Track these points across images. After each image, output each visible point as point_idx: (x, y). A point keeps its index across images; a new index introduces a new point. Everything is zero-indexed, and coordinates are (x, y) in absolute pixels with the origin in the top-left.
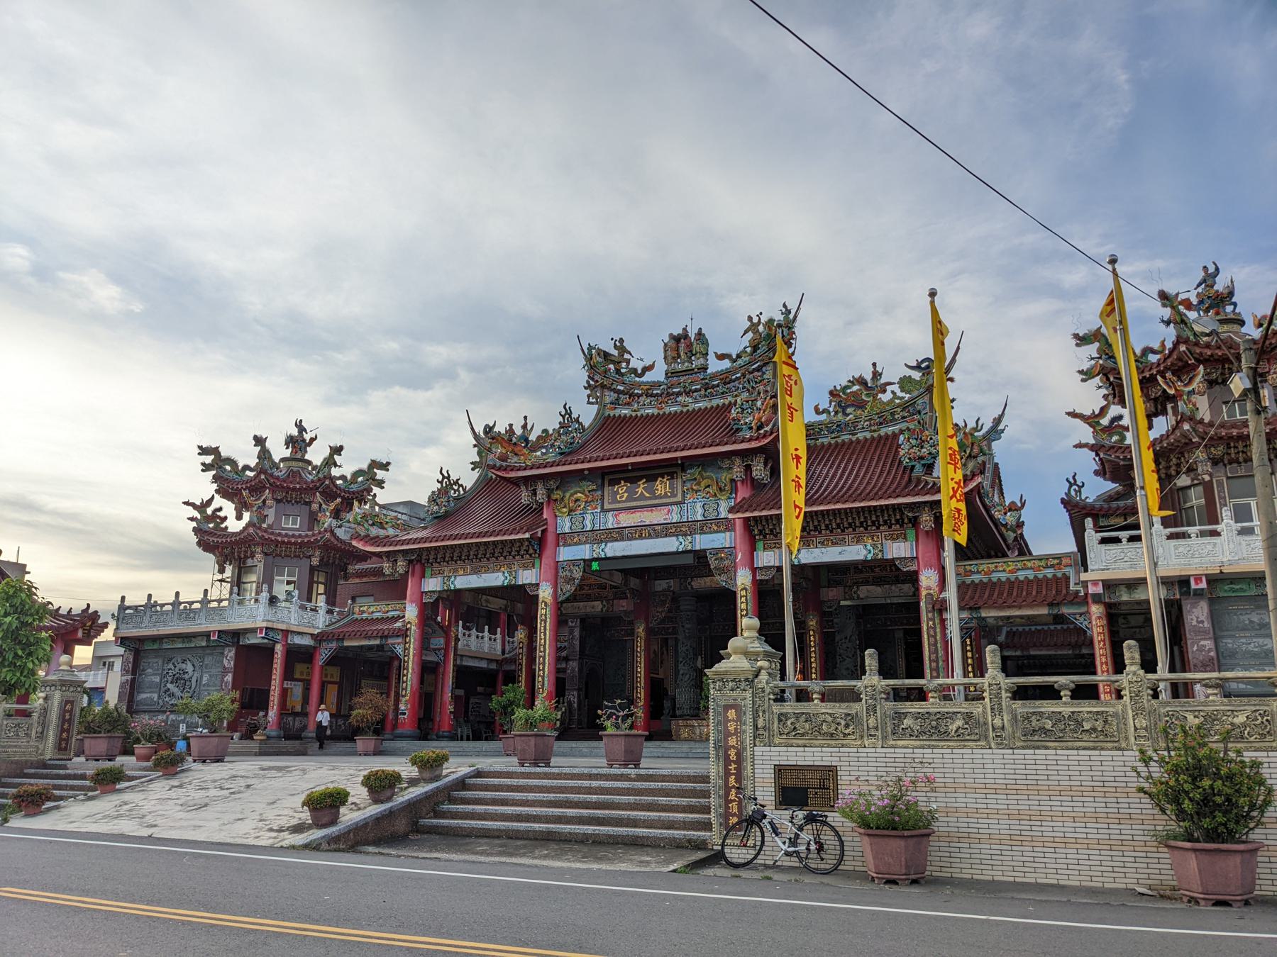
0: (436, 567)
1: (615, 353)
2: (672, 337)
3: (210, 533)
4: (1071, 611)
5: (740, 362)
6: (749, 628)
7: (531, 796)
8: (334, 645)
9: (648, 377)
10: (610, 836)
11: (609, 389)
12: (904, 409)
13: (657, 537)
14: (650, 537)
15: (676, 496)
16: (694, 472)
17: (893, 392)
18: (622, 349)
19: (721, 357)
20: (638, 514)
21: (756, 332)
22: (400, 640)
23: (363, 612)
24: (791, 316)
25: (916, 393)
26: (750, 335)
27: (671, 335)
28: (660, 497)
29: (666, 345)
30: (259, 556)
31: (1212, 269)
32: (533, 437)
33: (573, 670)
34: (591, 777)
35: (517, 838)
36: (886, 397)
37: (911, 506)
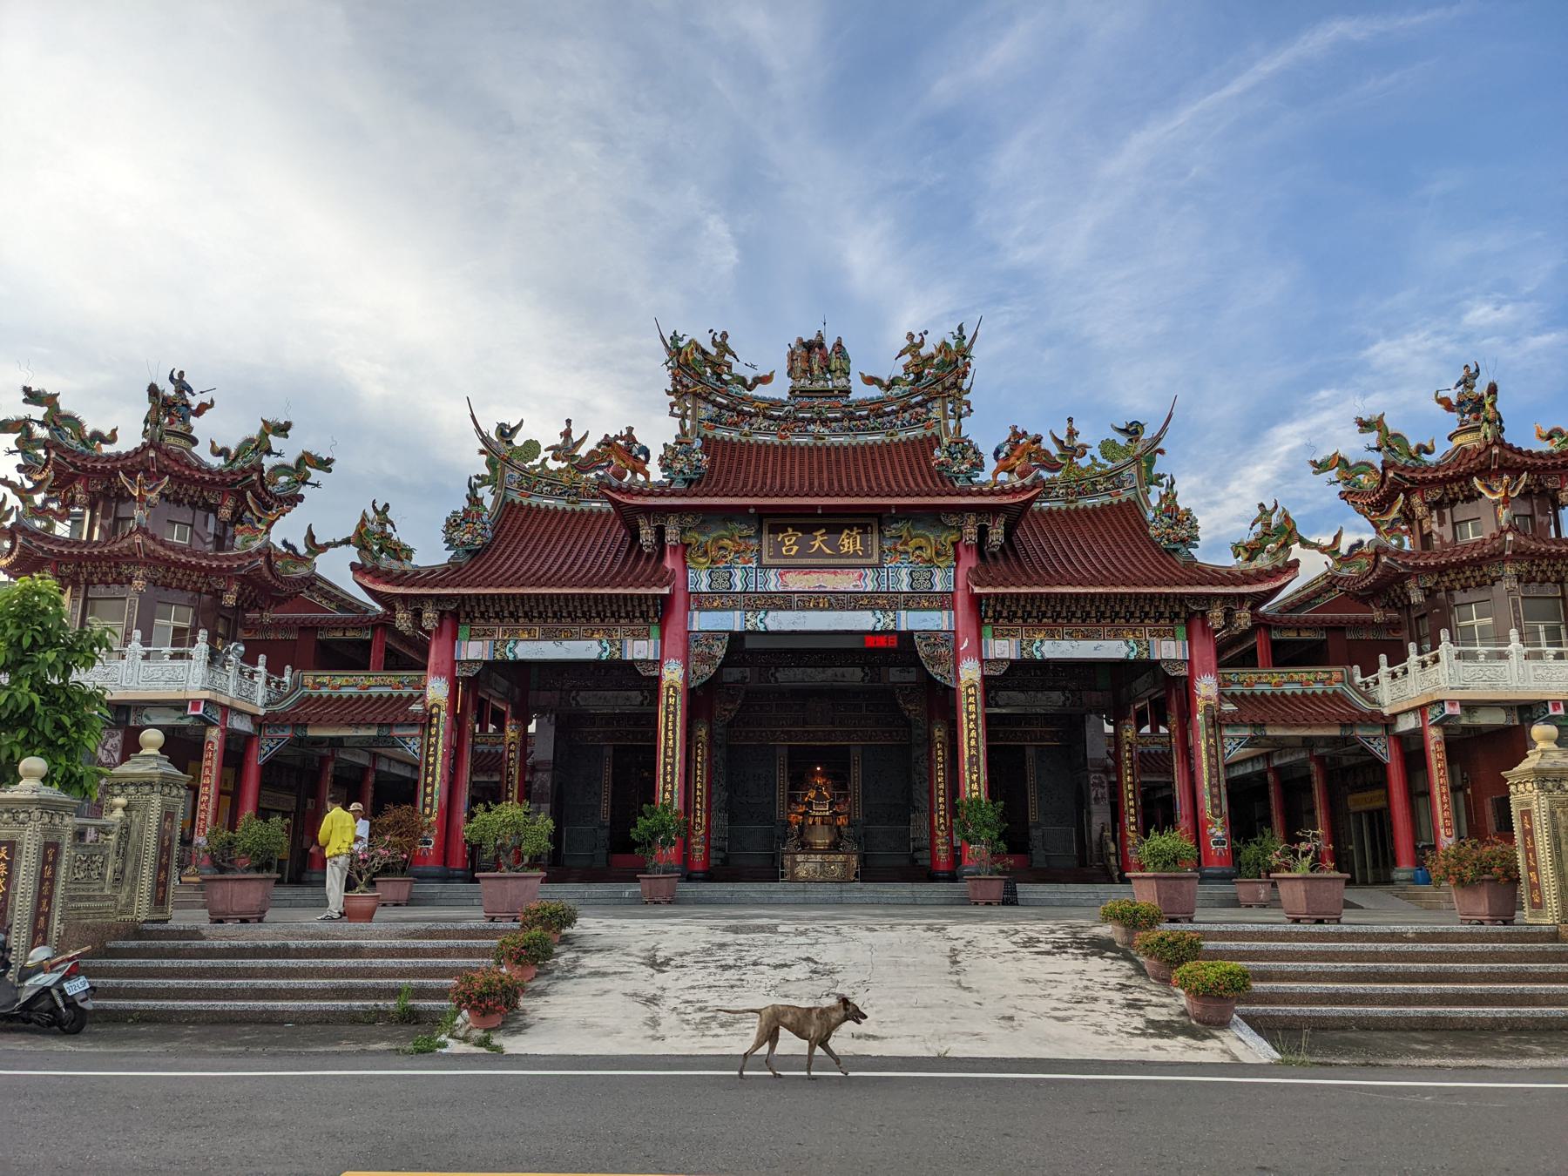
0: (480, 625)
1: (713, 351)
2: (801, 343)
3: (35, 534)
4: (1365, 734)
5: (896, 390)
6: (1547, 739)
7: (1312, 966)
8: (287, 733)
9: (760, 391)
10: (1538, 1020)
11: (706, 399)
12: (1108, 479)
13: (842, 609)
14: (831, 608)
15: (870, 556)
16: (902, 528)
18: (723, 347)
19: (870, 381)
22: (416, 731)
23: (323, 685)
24: (966, 342)
25: (1121, 462)
26: (907, 358)
27: (800, 339)
28: (847, 555)
29: (793, 352)
30: (139, 584)
31: (1472, 370)
34: (1264, 936)
35: (1378, 1029)
36: (1084, 462)
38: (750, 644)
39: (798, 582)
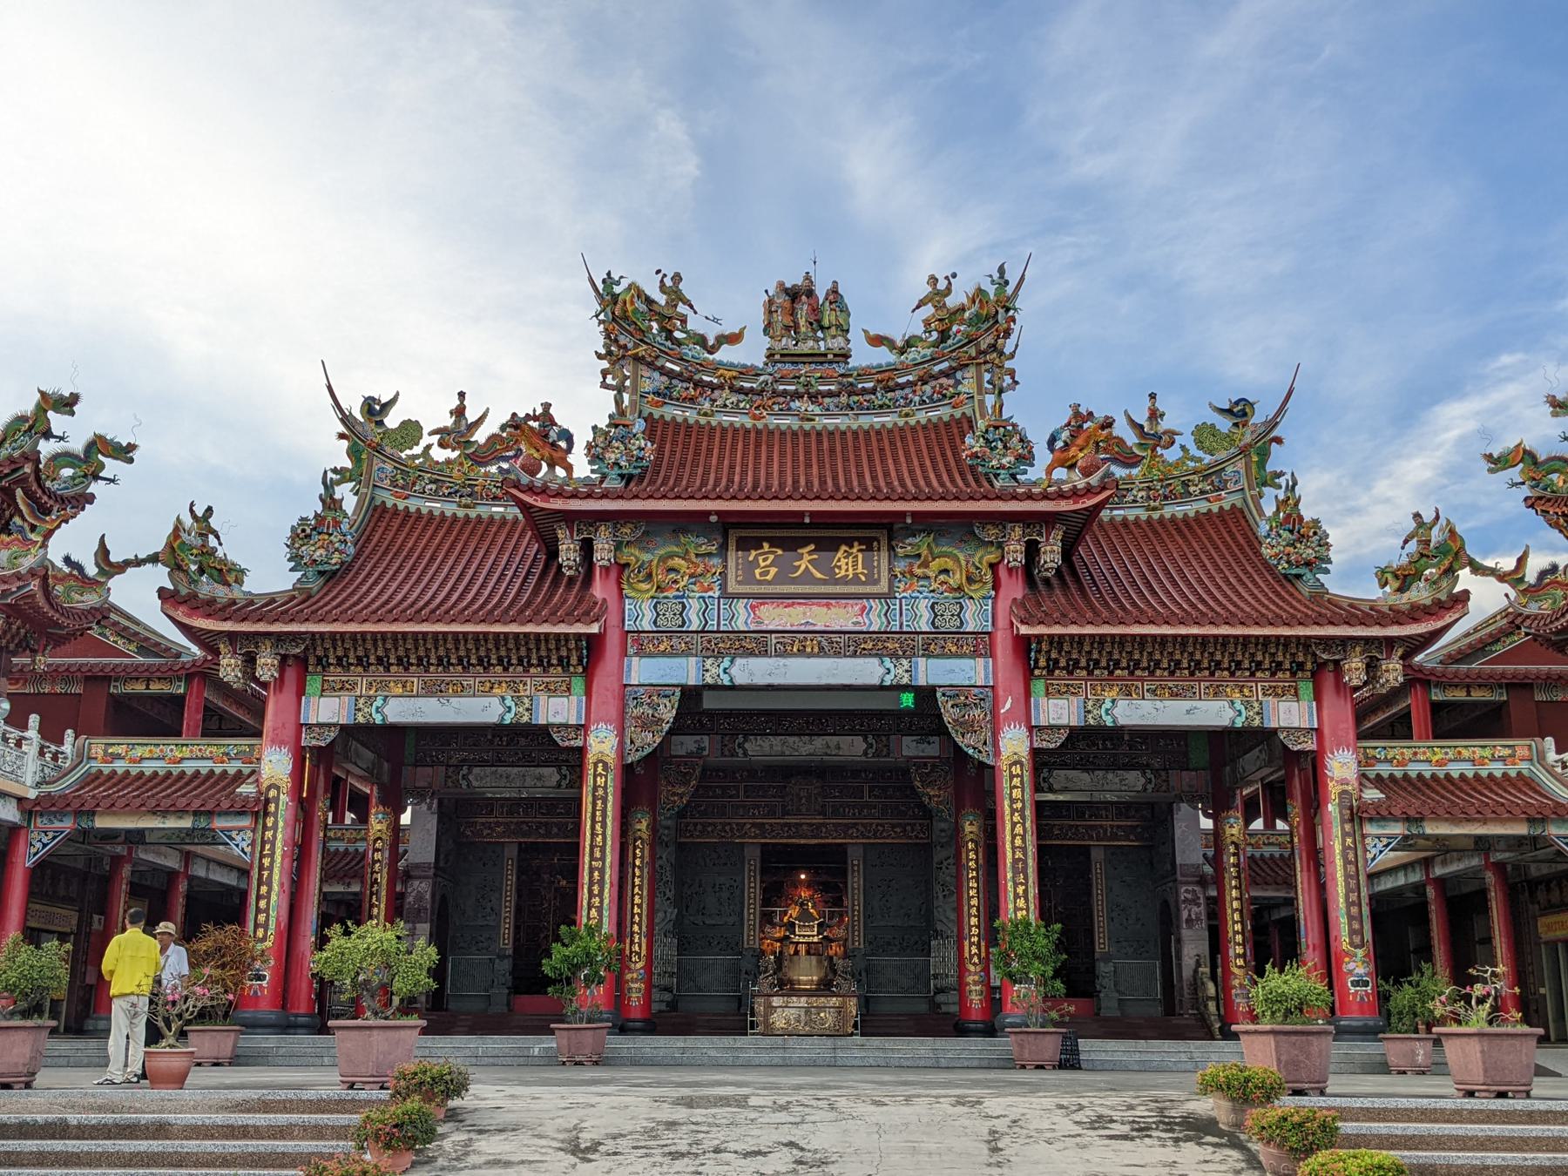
0: (335, 675)
1: (661, 299)
5: (912, 355)
8: (67, 824)
9: (725, 354)
11: (650, 365)
13: (837, 654)
15: (876, 582)
16: (920, 543)
17: (1183, 447)
19: (877, 341)
20: (801, 609)
21: (940, 307)
22: (246, 822)
24: (1010, 290)
25: (1223, 455)
26: (928, 310)
27: (781, 284)
28: (844, 581)
29: (771, 302)
32: (480, 436)
33: (420, 897)
36: (1172, 454)
37: (1327, 642)
38: (709, 702)
39: (775, 617)
